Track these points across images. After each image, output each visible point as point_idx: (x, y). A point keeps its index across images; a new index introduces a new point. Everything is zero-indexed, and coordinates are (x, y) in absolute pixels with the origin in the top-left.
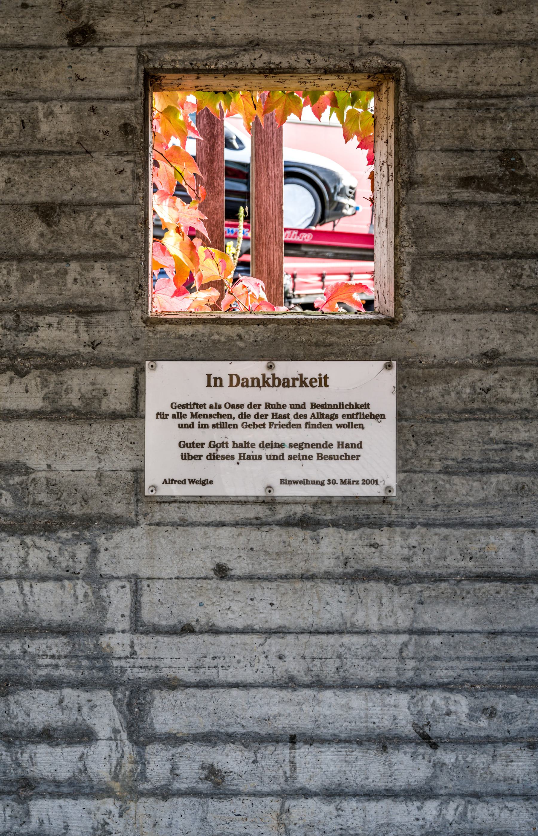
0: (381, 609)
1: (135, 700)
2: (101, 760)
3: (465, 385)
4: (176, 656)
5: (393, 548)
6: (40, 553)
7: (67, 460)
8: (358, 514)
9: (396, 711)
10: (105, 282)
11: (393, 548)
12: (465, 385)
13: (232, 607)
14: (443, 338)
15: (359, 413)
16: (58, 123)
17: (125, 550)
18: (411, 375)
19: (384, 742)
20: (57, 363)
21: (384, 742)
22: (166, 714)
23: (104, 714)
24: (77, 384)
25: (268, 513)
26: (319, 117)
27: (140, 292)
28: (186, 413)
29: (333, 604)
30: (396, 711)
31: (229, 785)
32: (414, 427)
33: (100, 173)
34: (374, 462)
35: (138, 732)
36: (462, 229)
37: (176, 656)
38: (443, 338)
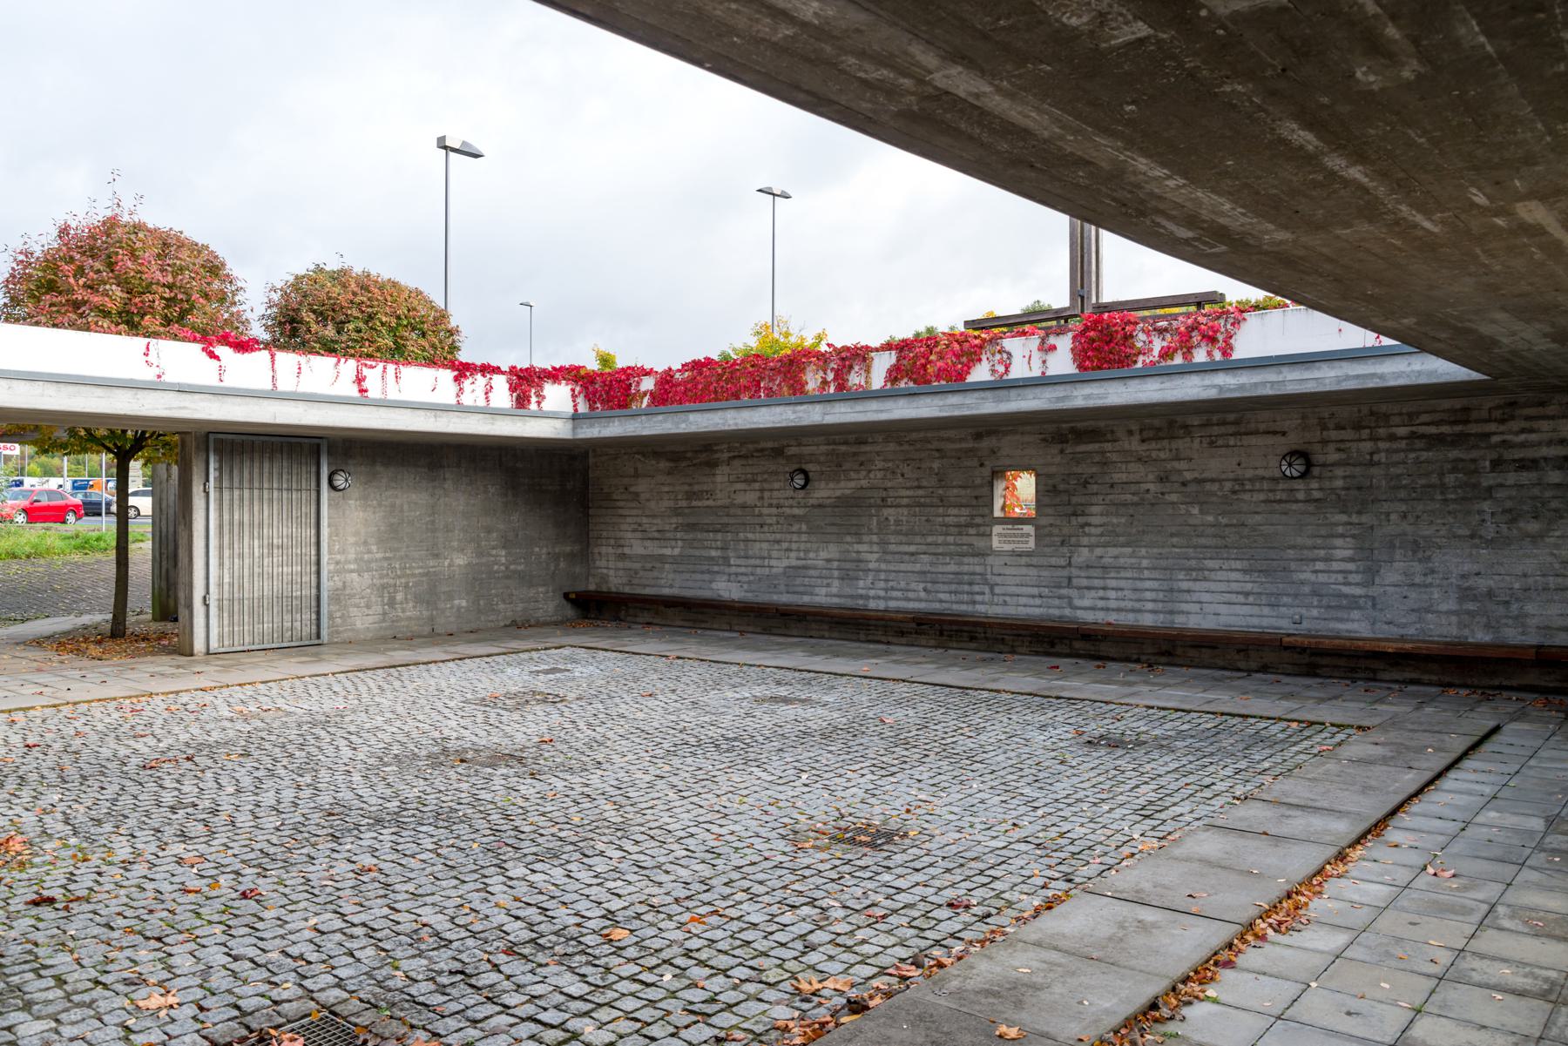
0: (1033, 572)
1: (992, 587)
2: (987, 598)
3: (1047, 530)
4: (998, 580)
5: (1035, 561)
6: (976, 560)
7: (980, 543)
8: (1029, 554)
9: (1035, 591)
10: (986, 511)
11: (1035, 561)
12: (1047, 530)
13: (1008, 571)
14: (1044, 521)
15: (1028, 535)
16: (978, 481)
17: (990, 560)
18: (1037, 528)
19: (1033, 597)
20: (978, 525)
21: (1033, 597)
22: (997, 590)
23: (987, 589)
24: (982, 529)
25: (1013, 553)
26: (1371, 574)
27: (992, 512)
28: (999, 535)
29: (1024, 571)
30: (1035, 591)
31: (463, 536)
32: (1038, 538)
33: (985, 490)
34: (1031, 544)
35: (993, 594)
36: (1046, 500)
37: (998, 580)
38: (1044, 521)
